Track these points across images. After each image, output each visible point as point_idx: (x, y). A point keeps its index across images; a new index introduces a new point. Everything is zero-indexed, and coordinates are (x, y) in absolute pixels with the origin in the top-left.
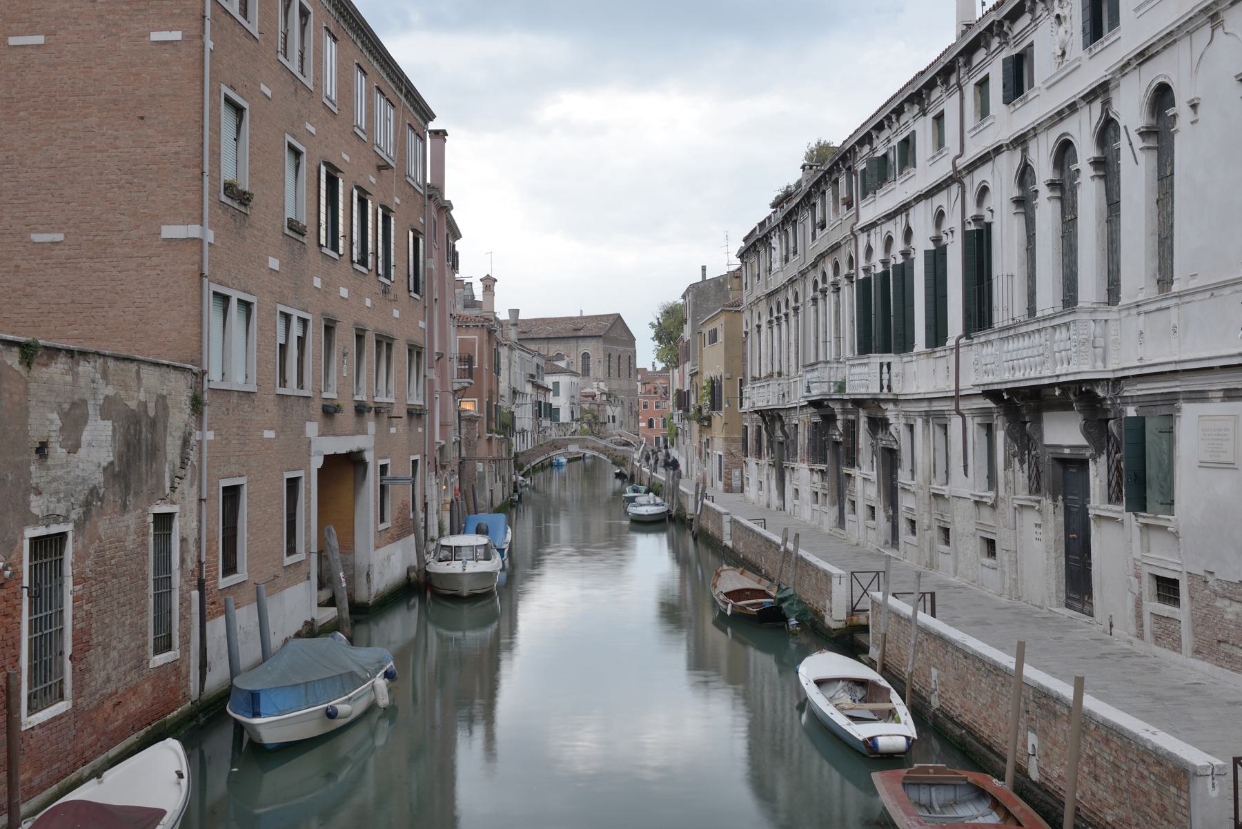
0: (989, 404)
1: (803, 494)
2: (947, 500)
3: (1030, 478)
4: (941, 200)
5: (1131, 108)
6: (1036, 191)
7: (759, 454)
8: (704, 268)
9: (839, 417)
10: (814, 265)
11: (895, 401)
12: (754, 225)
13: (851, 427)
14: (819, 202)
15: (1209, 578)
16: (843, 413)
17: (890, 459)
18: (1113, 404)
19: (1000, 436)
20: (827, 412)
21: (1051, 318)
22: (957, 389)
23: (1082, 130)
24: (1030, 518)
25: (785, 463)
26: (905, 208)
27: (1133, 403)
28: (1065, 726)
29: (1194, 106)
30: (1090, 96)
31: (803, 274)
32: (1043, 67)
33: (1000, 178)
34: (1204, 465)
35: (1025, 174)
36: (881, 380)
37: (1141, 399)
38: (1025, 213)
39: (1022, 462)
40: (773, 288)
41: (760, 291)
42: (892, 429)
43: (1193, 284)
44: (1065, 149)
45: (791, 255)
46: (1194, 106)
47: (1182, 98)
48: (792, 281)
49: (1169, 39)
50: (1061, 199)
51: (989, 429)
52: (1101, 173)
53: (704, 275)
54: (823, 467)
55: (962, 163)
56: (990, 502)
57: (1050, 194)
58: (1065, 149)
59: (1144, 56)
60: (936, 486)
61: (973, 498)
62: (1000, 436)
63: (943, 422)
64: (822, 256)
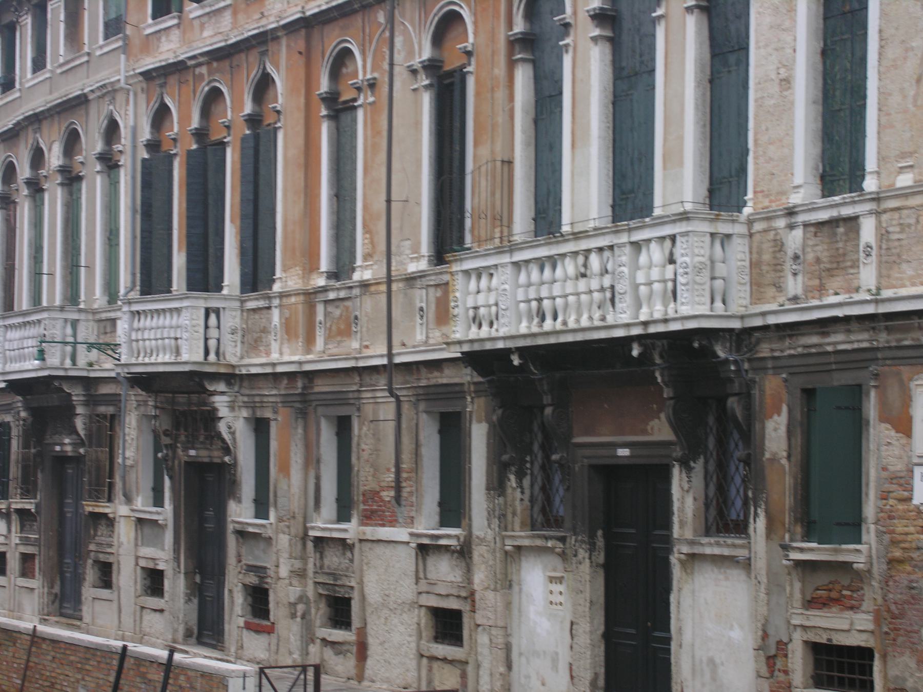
0: (466, 376)
1: (284, 593)
2: (351, 547)
3: (532, 500)
6: (567, 26)
9: (80, 410)
11: (231, 378)
13: (106, 431)
14: (27, 21)
16: (86, 404)
17: (202, 488)
18: (738, 371)
19: (479, 437)
20: (53, 400)
22: (390, 355)
25: (308, 525)
27: (777, 369)
36: (206, 339)
37: (796, 362)
38: (534, 62)
39: (520, 476)
42: (222, 427)
50: (614, 42)
51: (452, 431)
52: (608, 33)
54: (29, 505)
57: (597, 32)
60: (323, 523)
62: (479, 437)
63: (343, 411)
64: (36, 120)
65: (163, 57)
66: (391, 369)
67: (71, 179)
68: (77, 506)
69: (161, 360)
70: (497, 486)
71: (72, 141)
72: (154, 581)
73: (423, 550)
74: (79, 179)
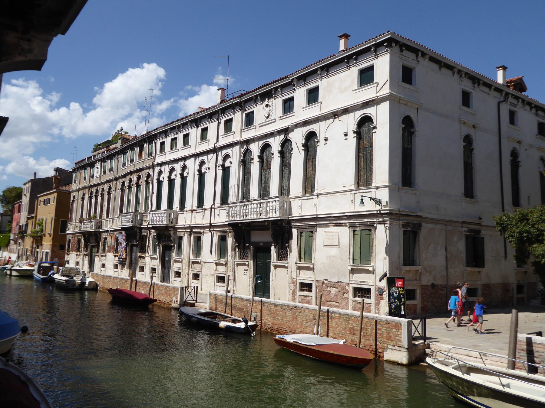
4: (205, 158)
5: (298, 137)
7: (78, 250)
8: (35, 174)
10: (124, 176)
12: (86, 157)
15: (325, 282)
19: (230, 240)
21: (254, 200)
23: (276, 143)
24: (241, 269)
26: (185, 159)
27: (295, 228)
28: (337, 320)
29: (326, 140)
30: (280, 132)
31: (116, 179)
32: (258, 118)
33: (235, 154)
34: (326, 246)
35: (247, 153)
40: (94, 183)
41: (85, 184)
43: (323, 192)
44: (266, 147)
45: (107, 172)
46: (326, 140)
47: (321, 137)
48: (108, 182)
49: (317, 120)
53: (35, 177)
55: (218, 145)
56: (224, 263)
58: (266, 147)
59: (306, 123)
61: (215, 262)
64: (131, 173)
65: (49, 220)
66: (210, 226)
67: (138, 186)
68: (136, 254)
69: (157, 223)
70: (233, 249)
71: (139, 178)
72: (154, 270)
73: (217, 264)
74: (140, 185)
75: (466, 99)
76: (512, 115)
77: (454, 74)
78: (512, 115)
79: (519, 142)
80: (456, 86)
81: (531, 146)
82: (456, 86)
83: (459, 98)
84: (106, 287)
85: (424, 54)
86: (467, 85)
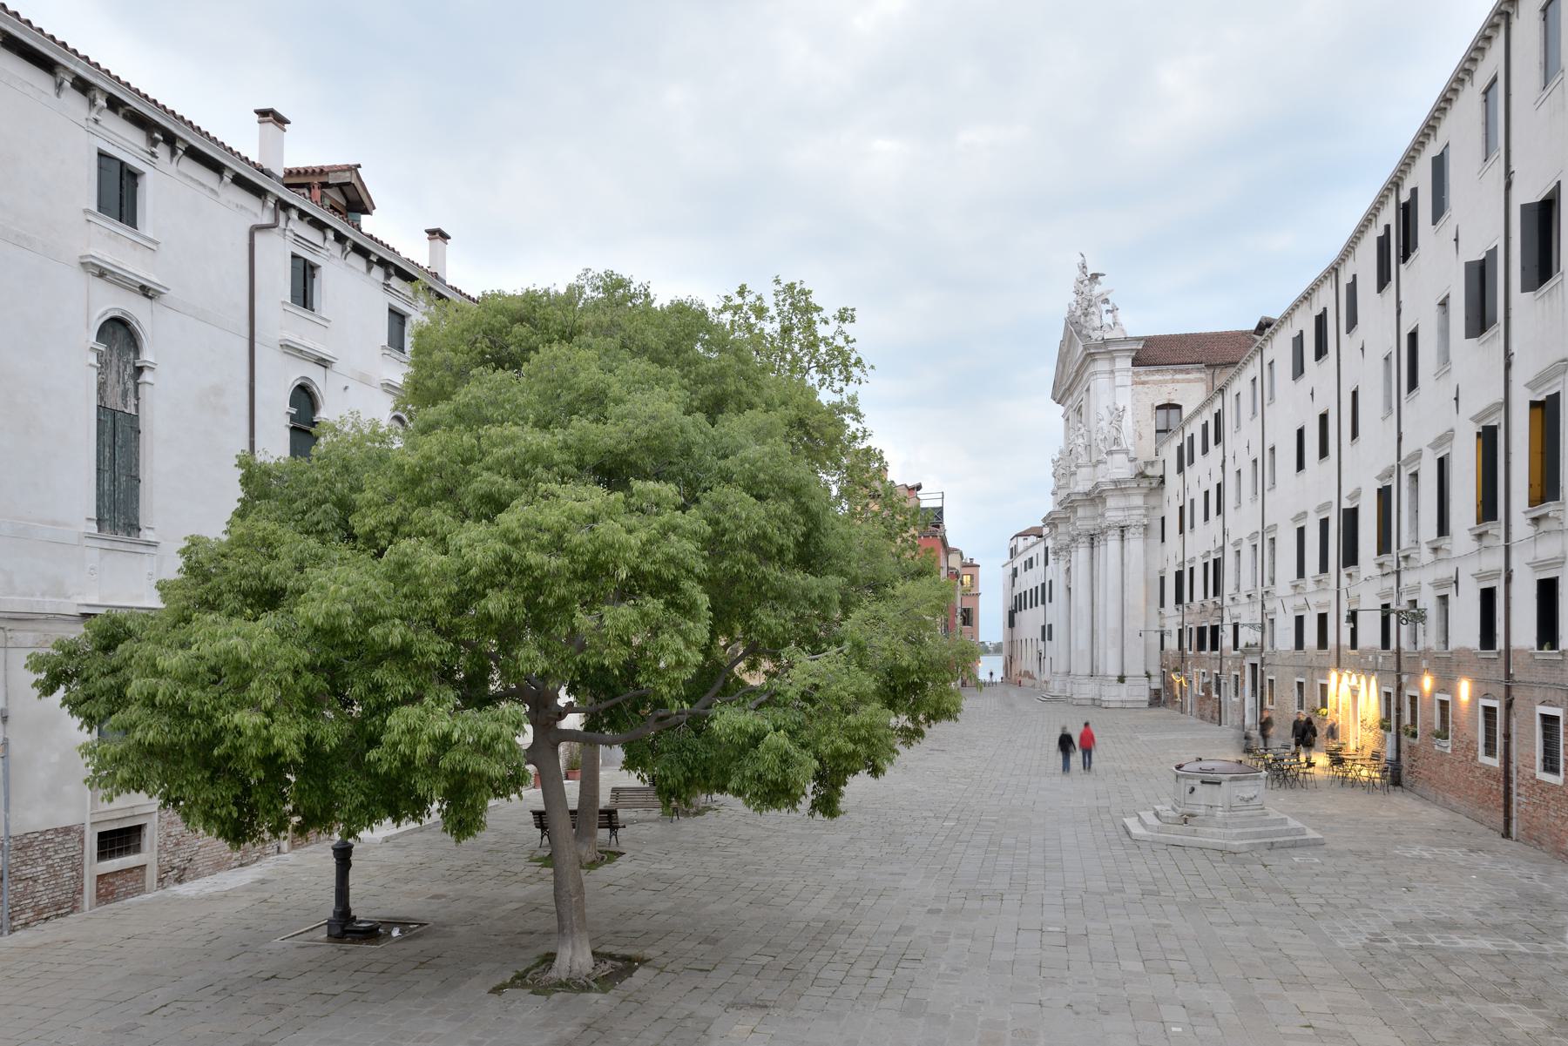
75: (119, 192)
76: (304, 276)
77: (59, 86)
78: (304, 276)
79: (323, 363)
80: (75, 139)
81: (364, 380)
82: (75, 139)
83: (85, 185)
84: (208, 879)
85: (170, 139)
86: (128, 144)
